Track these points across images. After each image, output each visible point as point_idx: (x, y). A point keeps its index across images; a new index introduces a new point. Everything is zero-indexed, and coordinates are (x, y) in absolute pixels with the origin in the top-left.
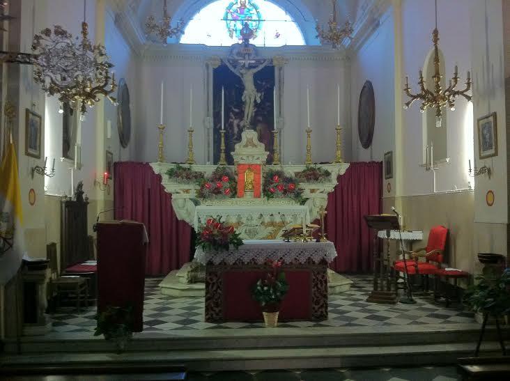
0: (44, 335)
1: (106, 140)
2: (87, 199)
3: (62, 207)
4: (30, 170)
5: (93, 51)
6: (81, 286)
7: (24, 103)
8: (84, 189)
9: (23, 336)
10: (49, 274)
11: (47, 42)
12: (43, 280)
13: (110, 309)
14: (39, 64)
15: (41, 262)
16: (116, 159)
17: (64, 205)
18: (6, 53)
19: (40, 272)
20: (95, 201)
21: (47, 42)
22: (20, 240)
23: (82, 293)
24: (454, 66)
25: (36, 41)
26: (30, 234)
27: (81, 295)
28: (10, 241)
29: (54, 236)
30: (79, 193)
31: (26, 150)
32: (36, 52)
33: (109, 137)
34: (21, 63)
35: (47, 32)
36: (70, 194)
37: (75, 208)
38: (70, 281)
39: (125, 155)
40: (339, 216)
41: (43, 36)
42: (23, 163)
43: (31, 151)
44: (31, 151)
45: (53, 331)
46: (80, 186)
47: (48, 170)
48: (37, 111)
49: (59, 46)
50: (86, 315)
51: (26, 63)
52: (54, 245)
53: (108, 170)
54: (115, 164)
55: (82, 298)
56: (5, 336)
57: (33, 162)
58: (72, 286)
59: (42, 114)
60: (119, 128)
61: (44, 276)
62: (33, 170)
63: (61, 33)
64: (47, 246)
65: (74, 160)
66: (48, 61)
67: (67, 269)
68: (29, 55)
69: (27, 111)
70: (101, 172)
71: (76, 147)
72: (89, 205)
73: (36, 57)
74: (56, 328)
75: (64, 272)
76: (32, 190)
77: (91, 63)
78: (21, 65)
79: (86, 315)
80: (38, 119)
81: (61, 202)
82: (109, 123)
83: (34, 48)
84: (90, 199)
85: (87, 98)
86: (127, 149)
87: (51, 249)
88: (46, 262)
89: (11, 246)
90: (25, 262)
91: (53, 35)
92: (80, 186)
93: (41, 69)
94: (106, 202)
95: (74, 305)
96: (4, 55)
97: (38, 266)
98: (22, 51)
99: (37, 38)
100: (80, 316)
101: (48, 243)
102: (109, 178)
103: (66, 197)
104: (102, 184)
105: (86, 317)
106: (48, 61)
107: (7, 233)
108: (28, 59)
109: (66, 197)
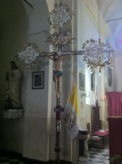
0: (87, 162)
1: (105, 84)
2: (99, 106)
3: (91, 109)
4: (81, 95)
5: (105, 46)
6: (100, 141)
7: (79, 71)
8: (98, 102)
9: (79, 161)
10: (89, 136)
11: (87, 45)
12: (86, 139)
13: (115, 157)
14: (85, 54)
15: (86, 132)
16: (108, 91)
17: (92, 108)
18: (73, 52)
19: (85, 135)
20: (102, 107)
21: (87, 45)
22: (78, 122)
23: (100, 144)
24: (82, 98)
25: (83, 46)
26: (82, 119)
27: (100, 144)
28: (74, 122)
29: (89, 120)
30: (97, 104)
31: (80, 87)
32: (84, 50)
33: (106, 83)
34: (78, 54)
35: (88, 42)
36: (94, 104)
37: (96, 110)
38: (96, 139)
39: (110, 90)
40: (116, 110)
41: (86, 43)
42: (79, 92)
43: (81, 88)
44: (81, 88)
45: (90, 161)
46: (97, 101)
47: (87, 95)
48: (83, 74)
49: (92, 46)
50: (102, 154)
51: (80, 54)
52: (89, 123)
53: (106, 95)
54: (108, 92)
55: (100, 145)
56: (73, 160)
57: (82, 92)
58: (96, 141)
59: (84, 75)
60: (108, 80)
61: (87, 137)
62: (82, 95)
63: (92, 41)
64: (87, 124)
65: (94, 91)
66: (88, 52)
67: (94, 133)
68: (81, 51)
69: (80, 73)
70: (103, 96)
71: (95, 87)
72: (100, 108)
73: (84, 52)
74: (92, 159)
75: (93, 134)
76: (82, 102)
77: (105, 51)
78: (78, 55)
79: (102, 154)
80: (83, 76)
81: (91, 107)
82: (106, 78)
83: (83, 48)
84: (101, 106)
85: (101, 67)
86: (111, 87)
87: (88, 125)
88: (87, 131)
89: (75, 124)
90: (80, 131)
91: (90, 43)
92: (97, 101)
93: (86, 56)
94: (105, 107)
95: (97, 148)
96: (73, 52)
97: (84, 133)
98: (78, 50)
99: (84, 44)
100: (99, 154)
101: (87, 123)
102: (106, 98)
103: (93, 105)
104: (104, 100)
105: (102, 155)
106: (88, 52)
107: (74, 119)
108: (81, 53)
109: (93, 105)
